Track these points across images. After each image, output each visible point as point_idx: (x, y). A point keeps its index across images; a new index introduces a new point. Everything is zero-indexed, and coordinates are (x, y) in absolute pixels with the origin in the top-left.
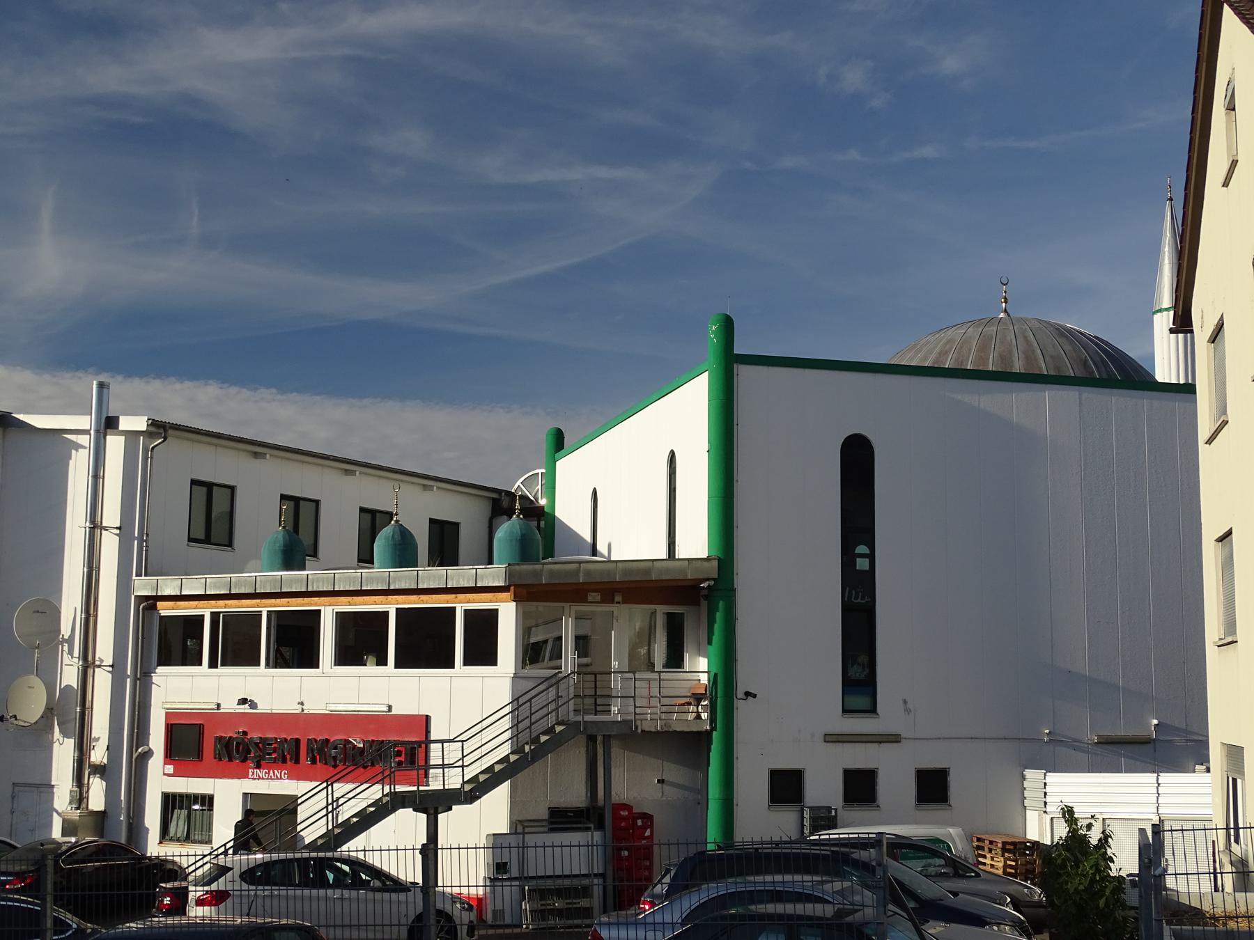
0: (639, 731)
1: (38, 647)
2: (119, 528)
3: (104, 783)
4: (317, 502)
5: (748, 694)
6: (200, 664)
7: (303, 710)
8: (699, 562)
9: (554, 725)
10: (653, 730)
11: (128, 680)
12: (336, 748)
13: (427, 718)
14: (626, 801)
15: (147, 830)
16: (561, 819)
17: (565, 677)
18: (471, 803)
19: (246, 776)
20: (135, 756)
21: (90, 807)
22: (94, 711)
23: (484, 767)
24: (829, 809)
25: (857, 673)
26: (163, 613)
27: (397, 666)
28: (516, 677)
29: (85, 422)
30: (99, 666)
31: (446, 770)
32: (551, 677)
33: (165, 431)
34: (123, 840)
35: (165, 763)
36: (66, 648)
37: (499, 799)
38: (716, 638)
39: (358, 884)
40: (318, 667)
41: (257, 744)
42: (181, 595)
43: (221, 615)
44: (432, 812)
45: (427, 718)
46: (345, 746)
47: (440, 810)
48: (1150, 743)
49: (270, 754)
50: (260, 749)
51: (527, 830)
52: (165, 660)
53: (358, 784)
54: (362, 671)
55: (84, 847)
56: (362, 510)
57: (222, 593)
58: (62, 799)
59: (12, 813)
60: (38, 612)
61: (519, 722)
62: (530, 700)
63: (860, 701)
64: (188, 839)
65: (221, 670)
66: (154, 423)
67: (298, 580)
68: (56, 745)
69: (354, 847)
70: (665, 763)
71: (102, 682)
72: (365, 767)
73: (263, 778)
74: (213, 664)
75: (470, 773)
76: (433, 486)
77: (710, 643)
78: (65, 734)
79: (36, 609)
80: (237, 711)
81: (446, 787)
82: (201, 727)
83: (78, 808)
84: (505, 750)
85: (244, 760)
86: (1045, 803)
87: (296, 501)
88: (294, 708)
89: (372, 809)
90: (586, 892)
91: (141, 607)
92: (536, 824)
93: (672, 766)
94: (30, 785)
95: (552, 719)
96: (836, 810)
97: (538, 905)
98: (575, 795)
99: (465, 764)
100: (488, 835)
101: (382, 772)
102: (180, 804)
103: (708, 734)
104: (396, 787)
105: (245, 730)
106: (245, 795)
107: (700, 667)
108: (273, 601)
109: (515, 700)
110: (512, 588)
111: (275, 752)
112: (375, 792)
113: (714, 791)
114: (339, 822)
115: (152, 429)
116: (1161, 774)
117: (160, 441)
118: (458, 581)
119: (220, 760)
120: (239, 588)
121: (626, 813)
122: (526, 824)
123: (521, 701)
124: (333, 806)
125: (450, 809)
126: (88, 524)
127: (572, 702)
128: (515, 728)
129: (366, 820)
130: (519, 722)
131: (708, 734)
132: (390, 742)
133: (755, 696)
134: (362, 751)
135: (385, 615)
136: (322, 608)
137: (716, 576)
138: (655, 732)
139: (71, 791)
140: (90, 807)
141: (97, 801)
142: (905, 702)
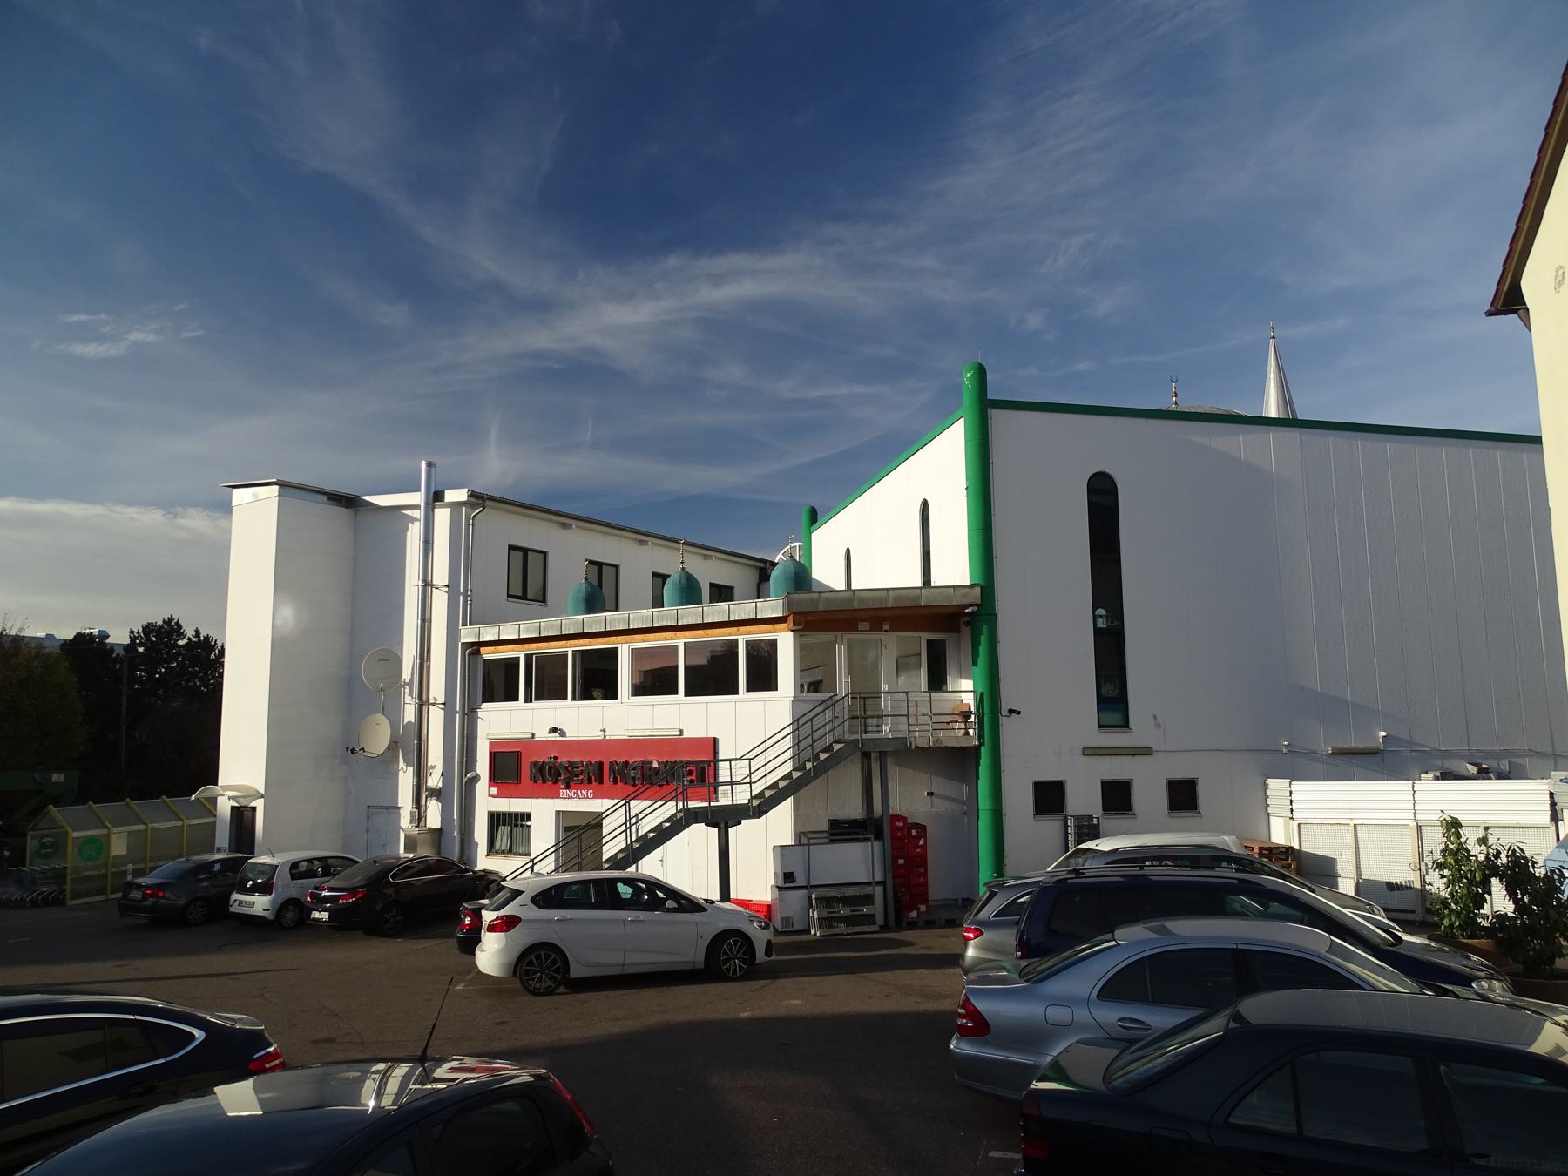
0: (913, 747)
1: (382, 689)
2: (448, 586)
3: (440, 804)
4: (617, 567)
5: (1011, 711)
6: (517, 700)
7: (605, 737)
8: (964, 590)
9: (831, 744)
10: (926, 746)
11: (458, 715)
12: (634, 769)
13: (715, 740)
14: (899, 813)
15: (477, 844)
16: (841, 831)
17: (841, 699)
18: (759, 818)
19: (558, 796)
20: (465, 780)
21: (428, 825)
22: (429, 744)
23: (768, 784)
24: (1090, 818)
25: (1110, 690)
26: (486, 657)
27: (687, 694)
28: (795, 700)
29: (418, 498)
30: (433, 704)
31: (734, 786)
32: (828, 700)
33: (483, 501)
34: (455, 857)
35: (489, 787)
36: (407, 690)
37: (783, 814)
38: (982, 659)
39: (656, 904)
40: (617, 698)
41: (566, 768)
42: (499, 640)
43: (534, 657)
44: (723, 826)
45: (715, 740)
46: (642, 767)
47: (730, 823)
48: (1377, 753)
49: (578, 776)
50: (569, 772)
51: (812, 841)
52: (489, 697)
53: (652, 802)
54: (656, 700)
55: (421, 861)
56: (655, 574)
57: (533, 636)
58: (405, 821)
59: (368, 831)
60: (382, 660)
61: (799, 742)
62: (811, 720)
63: (1115, 717)
64: (510, 852)
65: (535, 704)
66: (472, 495)
67: (597, 622)
68: (401, 773)
69: (649, 866)
70: (933, 777)
71: (436, 717)
72: (661, 786)
73: (572, 798)
74: (528, 700)
75: (757, 789)
76: (711, 556)
77: (975, 663)
78: (408, 764)
79: (381, 658)
80: (549, 739)
81: (735, 803)
82: (519, 753)
83: (417, 827)
84: (788, 767)
85: (556, 782)
86: (1292, 810)
87: (600, 565)
88: (598, 735)
89: (667, 825)
90: (868, 899)
91: (467, 652)
92: (817, 836)
93: (940, 779)
94: (382, 807)
95: (829, 739)
96: (1098, 818)
97: (825, 914)
98: (853, 809)
99: (753, 781)
100: (774, 846)
101: (676, 790)
102: (863, 625)
103: (977, 749)
104: (689, 803)
105: (556, 755)
106: (558, 812)
107: (964, 690)
108: (577, 642)
109: (795, 721)
110: (791, 618)
111: (581, 774)
112: (670, 808)
113: (984, 803)
114: (640, 835)
115: (472, 499)
116: (1416, 782)
117: (479, 510)
118: (739, 614)
119: (535, 782)
120: (548, 631)
121: (901, 824)
122: (809, 836)
123: (801, 722)
124: (628, 824)
125: (740, 823)
126: (420, 583)
127: (847, 723)
128: (796, 747)
129: (663, 835)
130: (799, 742)
131: (977, 749)
132: (682, 762)
133: (1019, 713)
134: (657, 771)
135: (676, 648)
136: (619, 646)
137: (979, 602)
138: (927, 748)
139: (411, 812)
140: (428, 825)
141: (434, 819)
142: (1155, 717)
